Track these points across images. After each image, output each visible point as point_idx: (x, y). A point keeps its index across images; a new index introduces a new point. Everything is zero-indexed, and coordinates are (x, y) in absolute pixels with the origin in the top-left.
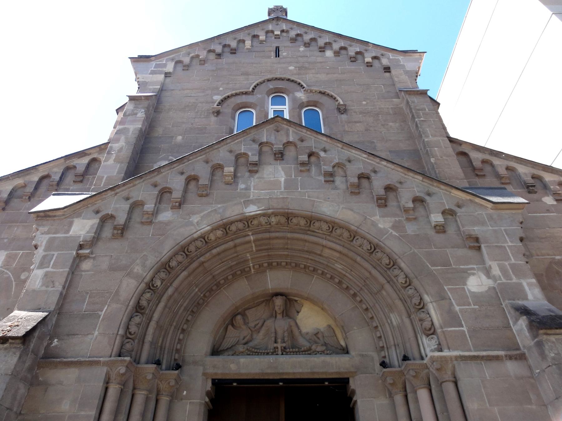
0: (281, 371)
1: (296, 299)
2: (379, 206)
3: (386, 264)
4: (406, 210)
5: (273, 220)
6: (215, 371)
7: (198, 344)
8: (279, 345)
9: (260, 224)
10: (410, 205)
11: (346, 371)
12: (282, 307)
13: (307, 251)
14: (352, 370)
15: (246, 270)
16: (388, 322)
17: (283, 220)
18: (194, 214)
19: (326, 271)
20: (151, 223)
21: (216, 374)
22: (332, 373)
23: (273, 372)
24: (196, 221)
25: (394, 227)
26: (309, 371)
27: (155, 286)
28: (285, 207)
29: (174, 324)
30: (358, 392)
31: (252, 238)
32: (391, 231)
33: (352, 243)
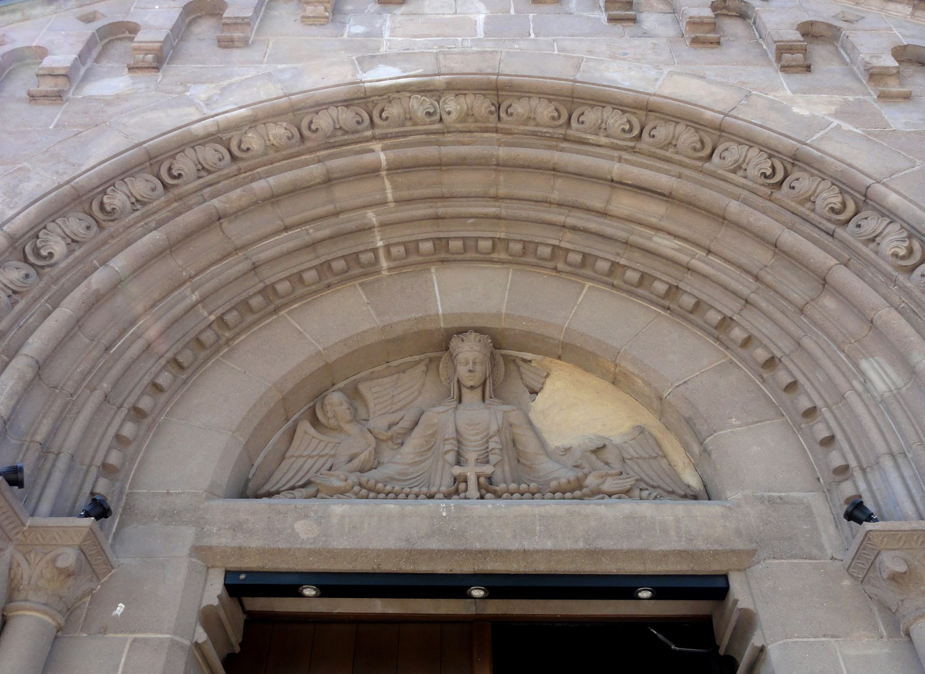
0: (478, 546)
1: (528, 356)
2: (786, 69)
3: (832, 210)
4: (875, 75)
5: (453, 106)
6: (240, 540)
7: (192, 453)
8: (471, 471)
9: (409, 118)
10: (890, 62)
11: (716, 547)
12: (479, 368)
13: (560, 205)
14: (739, 545)
15: (364, 258)
16: (853, 388)
17: (482, 106)
18: (197, 81)
19: (623, 261)
20: (58, 97)
21: (240, 551)
22: (665, 555)
23: (449, 546)
24: (203, 96)
25: (840, 114)
26: (581, 545)
27: (44, 253)
28: (489, 71)
29: (106, 385)
30: (766, 616)
31: (383, 156)
32: (836, 122)
33: (707, 165)
